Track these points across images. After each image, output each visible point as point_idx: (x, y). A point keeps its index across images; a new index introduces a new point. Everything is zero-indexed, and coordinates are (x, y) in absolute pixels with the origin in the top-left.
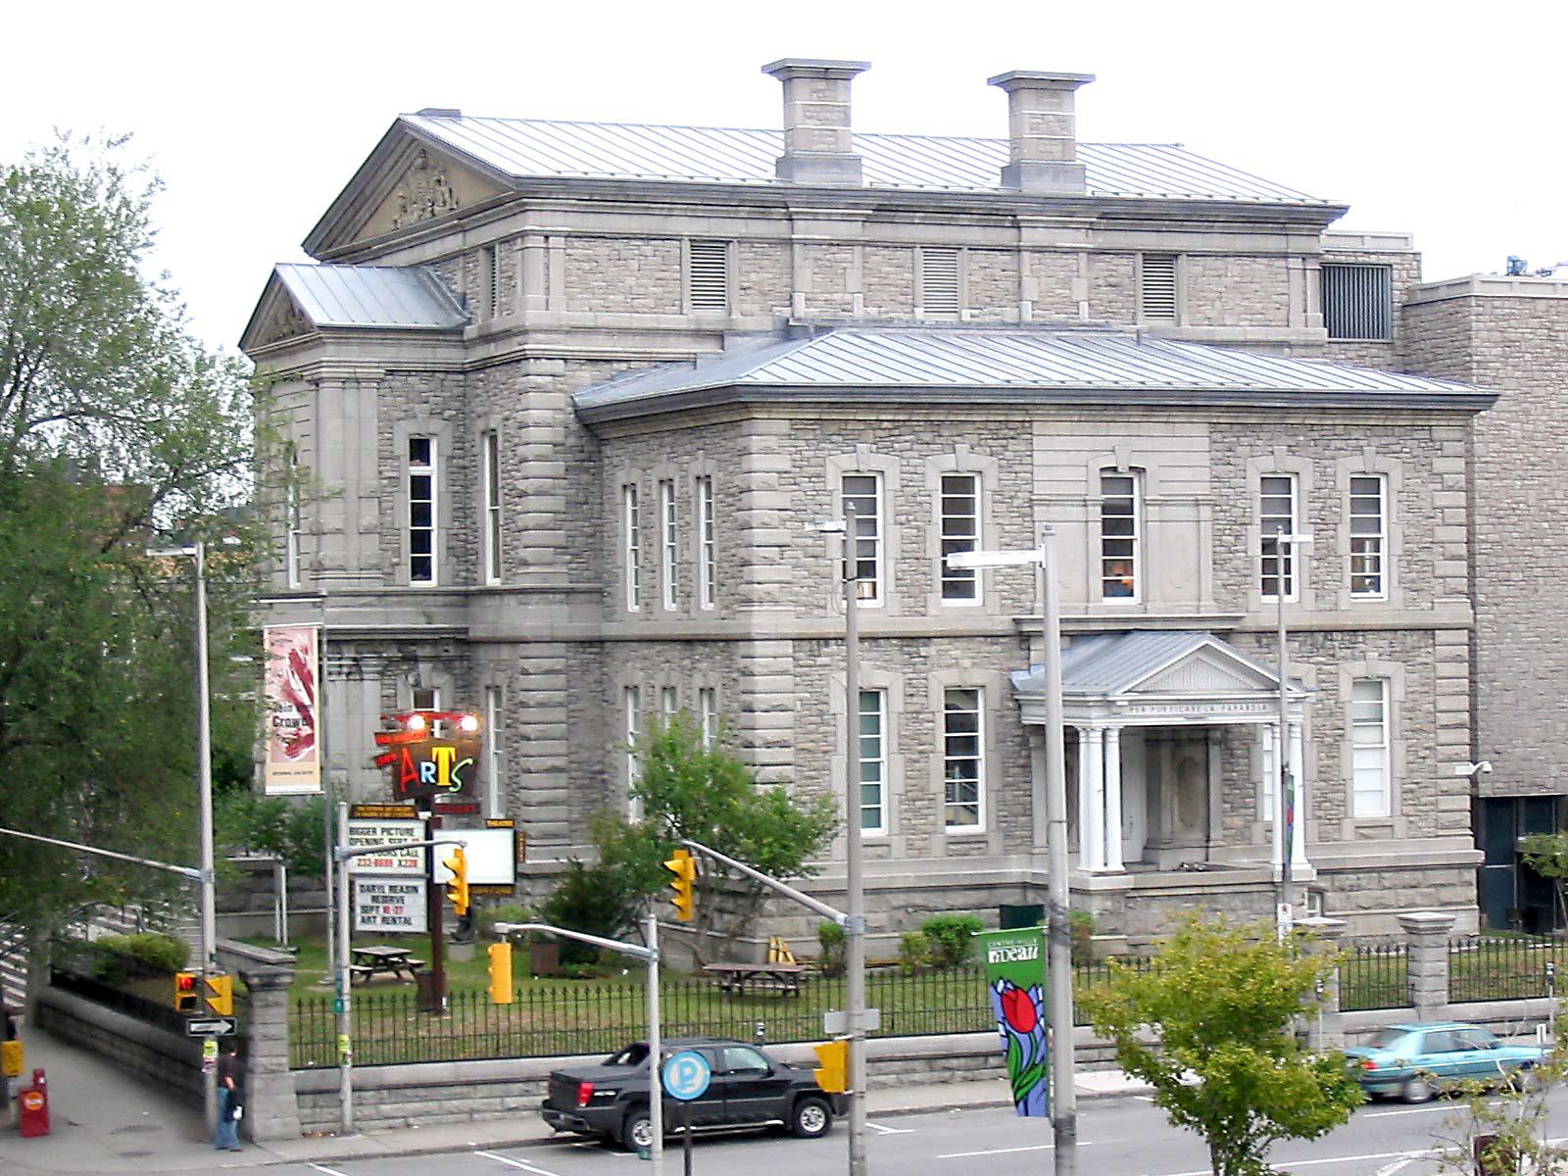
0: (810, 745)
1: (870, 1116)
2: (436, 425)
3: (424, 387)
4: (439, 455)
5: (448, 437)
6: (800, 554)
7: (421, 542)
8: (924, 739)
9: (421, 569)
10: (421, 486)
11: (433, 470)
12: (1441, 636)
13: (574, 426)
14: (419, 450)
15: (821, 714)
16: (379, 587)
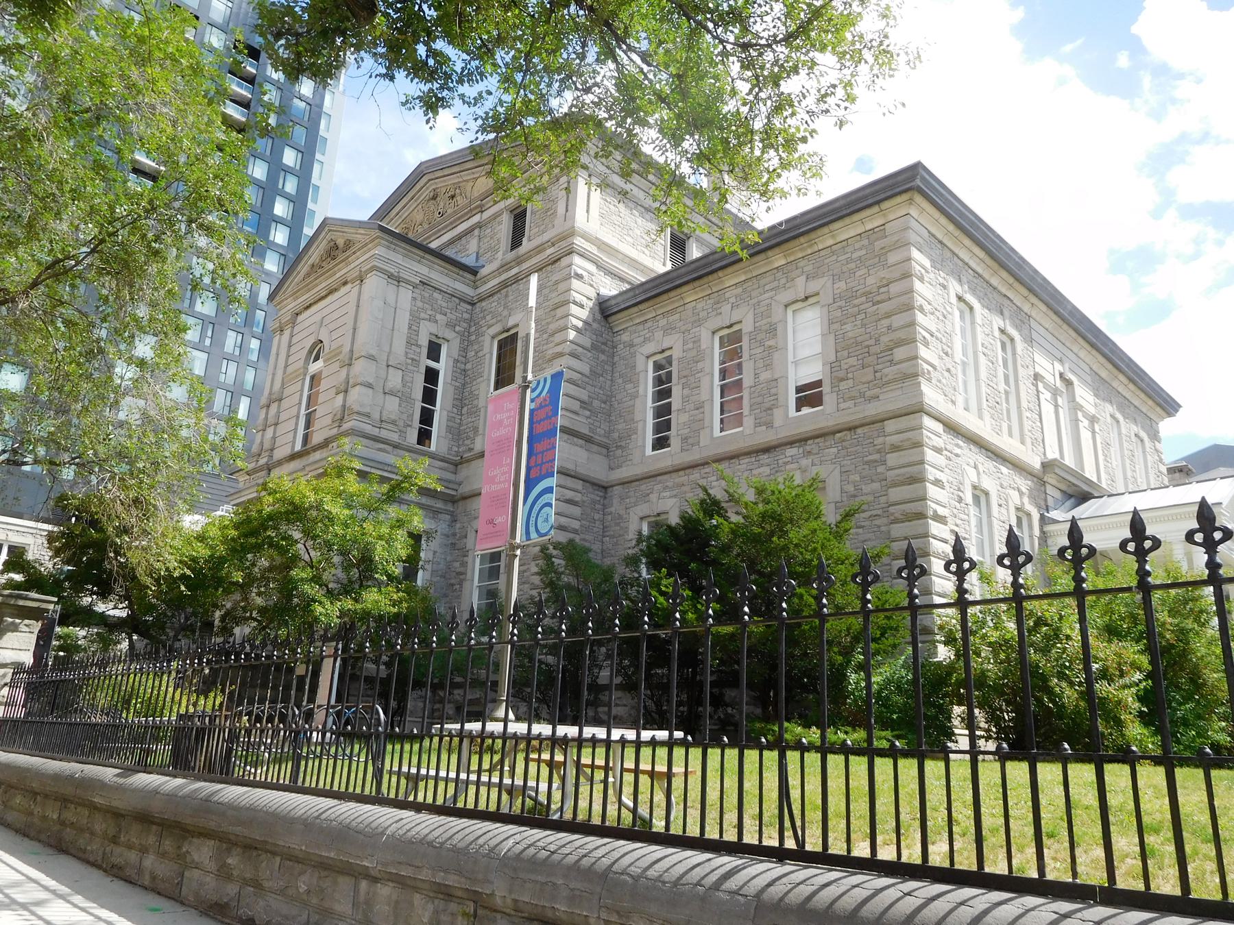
1: (582, 306)
2: (449, 334)
3: (444, 304)
4: (448, 356)
5: (456, 343)
7: (427, 417)
9: (424, 436)
10: (431, 376)
11: (442, 366)
13: (598, 316)
14: (434, 351)
16: (395, 437)
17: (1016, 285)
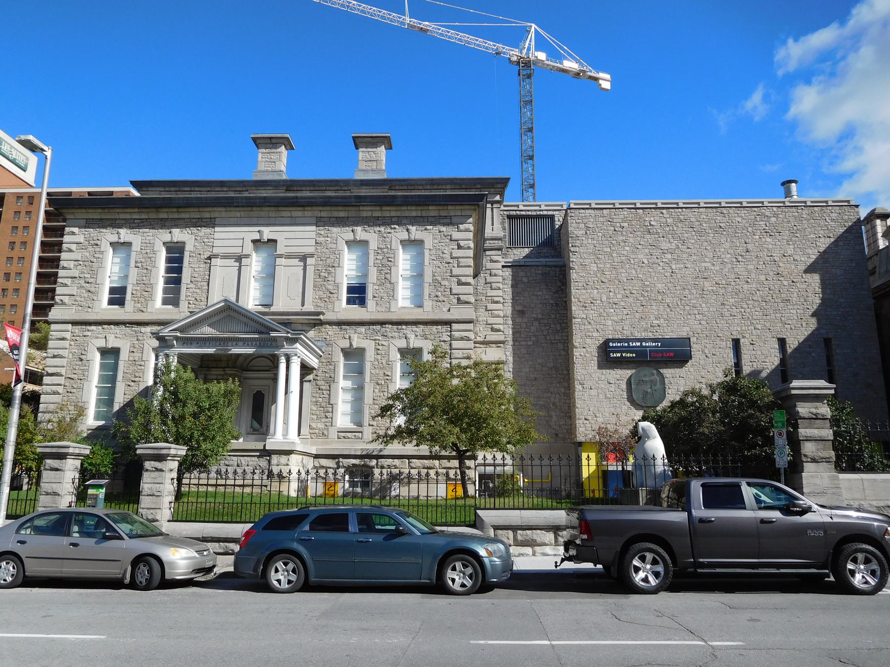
0: (72, 376)
6: (82, 282)
8: (137, 374)
12: (455, 326)
15: (81, 360)
17: (180, 210)
